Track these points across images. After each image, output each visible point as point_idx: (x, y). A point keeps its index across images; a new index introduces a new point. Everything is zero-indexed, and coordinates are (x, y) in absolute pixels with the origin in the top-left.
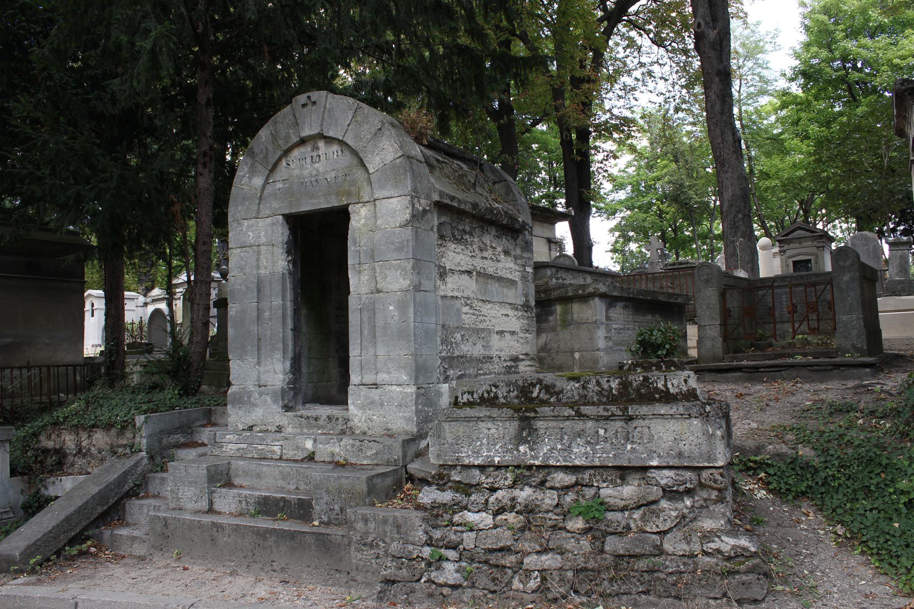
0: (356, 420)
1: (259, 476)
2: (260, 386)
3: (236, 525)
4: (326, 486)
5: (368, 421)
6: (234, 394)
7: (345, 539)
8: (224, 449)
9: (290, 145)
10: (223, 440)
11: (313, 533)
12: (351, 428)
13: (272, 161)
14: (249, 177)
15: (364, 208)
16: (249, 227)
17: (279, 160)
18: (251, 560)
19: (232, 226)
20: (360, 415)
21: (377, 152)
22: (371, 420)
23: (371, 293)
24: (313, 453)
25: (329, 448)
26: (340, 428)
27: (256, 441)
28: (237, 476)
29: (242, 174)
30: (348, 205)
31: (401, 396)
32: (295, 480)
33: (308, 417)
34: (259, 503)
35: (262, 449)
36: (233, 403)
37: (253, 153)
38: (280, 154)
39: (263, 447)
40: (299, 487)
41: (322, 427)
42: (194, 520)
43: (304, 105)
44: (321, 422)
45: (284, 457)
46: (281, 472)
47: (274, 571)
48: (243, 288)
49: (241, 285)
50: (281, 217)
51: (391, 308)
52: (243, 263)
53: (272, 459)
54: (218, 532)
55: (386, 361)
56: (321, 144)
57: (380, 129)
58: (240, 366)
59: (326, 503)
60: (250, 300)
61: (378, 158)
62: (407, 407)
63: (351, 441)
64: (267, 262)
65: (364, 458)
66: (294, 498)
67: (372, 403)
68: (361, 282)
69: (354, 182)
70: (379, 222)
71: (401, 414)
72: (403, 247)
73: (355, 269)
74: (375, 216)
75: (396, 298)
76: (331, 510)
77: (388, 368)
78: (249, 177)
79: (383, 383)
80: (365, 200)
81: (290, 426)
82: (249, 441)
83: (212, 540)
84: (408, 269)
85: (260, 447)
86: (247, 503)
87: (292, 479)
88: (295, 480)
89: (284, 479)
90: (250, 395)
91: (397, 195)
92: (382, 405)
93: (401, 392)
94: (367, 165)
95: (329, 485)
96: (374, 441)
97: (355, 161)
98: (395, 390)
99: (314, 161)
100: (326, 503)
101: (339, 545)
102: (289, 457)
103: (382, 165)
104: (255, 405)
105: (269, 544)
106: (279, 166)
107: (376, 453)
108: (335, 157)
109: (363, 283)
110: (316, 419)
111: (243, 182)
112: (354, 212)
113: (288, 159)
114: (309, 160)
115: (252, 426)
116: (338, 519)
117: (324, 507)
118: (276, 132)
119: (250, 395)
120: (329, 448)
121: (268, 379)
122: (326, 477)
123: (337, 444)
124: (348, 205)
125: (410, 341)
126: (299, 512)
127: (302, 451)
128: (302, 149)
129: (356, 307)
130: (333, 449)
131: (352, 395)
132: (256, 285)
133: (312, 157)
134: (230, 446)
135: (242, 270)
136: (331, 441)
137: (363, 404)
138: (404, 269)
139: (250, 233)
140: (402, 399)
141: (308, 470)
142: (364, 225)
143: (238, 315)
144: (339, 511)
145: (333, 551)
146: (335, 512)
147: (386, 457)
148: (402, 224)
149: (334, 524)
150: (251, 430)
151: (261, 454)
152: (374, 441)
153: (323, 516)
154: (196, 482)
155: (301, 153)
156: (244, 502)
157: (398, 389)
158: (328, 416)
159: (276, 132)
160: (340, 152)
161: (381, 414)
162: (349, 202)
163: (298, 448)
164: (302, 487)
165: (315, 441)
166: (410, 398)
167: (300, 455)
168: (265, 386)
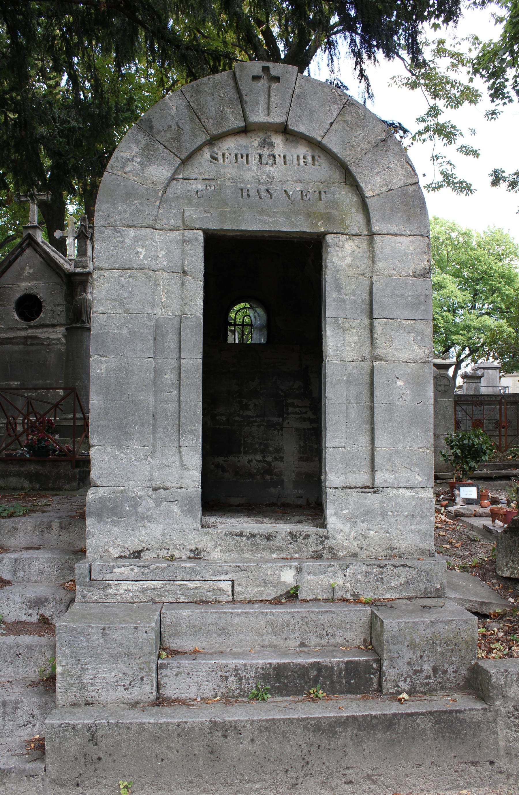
0: (340, 538)
1: (224, 631)
2: (155, 489)
3: (267, 721)
4: (408, 638)
5: (360, 538)
6: (102, 501)
7: (489, 714)
8: (112, 591)
9: (225, 129)
10: (108, 577)
11: (431, 713)
12: (331, 549)
13: (189, 146)
14: (141, 163)
15: (350, 243)
16: (136, 239)
17: (200, 148)
18: (301, 774)
19: (101, 232)
20: (346, 529)
21: (377, 170)
22: (365, 537)
23: (362, 361)
24: (297, 588)
25: (326, 580)
26: (312, 549)
27: (180, 576)
28: (177, 634)
29: (126, 155)
30: (325, 234)
31: (414, 503)
32: (298, 633)
33: (253, 536)
34: (265, 677)
35: (196, 588)
36: (100, 515)
37: (151, 128)
38: (204, 139)
39: (198, 584)
40: (307, 643)
41: (280, 549)
42: (168, 724)
43: (256, 78)
44: (277, 542)
45: (238, 598)
46: (270, 623)
47: (351, 782)
48: (125, 332)
49: (120, 328)
50: (201, 233)
51: (400, 383)
52: (125, 294)
53: (217, 602)
54: (225, 737)
55: (390, 455)
56: (278, 140)
57: (383, 141)
58: (116, 457)
59: (409, 663)
60: (139, 354)
61: (378, 179)
62: (422, 517)
63: (364, 568)
64: (168, 297)
65: (386, 590)
66: (338, 663)
67: (369, 512)
68: (346, 344)
69: (335, 204)
70: (380, 265)
71: (413, 527)
72: (419, 304)
73: (339, 325)
74: (373, 257)
75: (408, 370)
76: (416, 672)
77: (393, 465)
78: (141, 163)
79: (385, 485)
80: (354, 232)
81: (218, 549)
82: (166, 575)
83: (212, 752)
84: (426, 333)
85: (191, 585)
86: (240, 679)
87: (294, 631)
88: (298, 633)
89: (276, 633)
90: (136, 502)
91: (409, 233)
92: (384, 515)
93: (413, 498)
94: (362, 185)
95: (415, 636)
96: (403, 565)
97: (337, 175)
98: (404, 495)
99: (264, 161)
100: (409, 663)
101: (478, 724)
102: (249, 597)
103: (385, 188)
104: (145, 518)
105: (340, 742)
106: (198, 157)
107: (407, 583)
108: (302, 163)
109: (349, 346)
110: (268, 538)
111: (127, 169)
112: (336, 245)
113: (216, 150)
114: (254, 160)
115: (140, 552)
116: (428, 684)
117: (405, 669)
118: (198, 105)
119: (136, 502)
120: (326, 580)
121: (169, 478)
122: (410, 625)
123: (340, 573)
124: (325, 234)
125: (428, 430)
126: (348, 682)
127: (274, 586)
128: (242, 141)
129: (339, 377)
130: (332, 582)
131: (334, 502)
132: (152, 330)
133: (260, 156)
134: (125, 585)
135: (122, 304)
136: (329, 569)
137: (353, 514)
138: (420, 333)
139: (139, 249)
140: (416, 506)
141: (325, 615)
142: (350, 265)
143: (113, 375)
144: (431, 673)
145: (465, 735)
146: (424, 674)
147: (422, 586)
148: (418, 273)
149: (422, 692)
150: (139, 557)
151: (195, 595)
152: (403, 565)
153: (401, 684)
154: (129, 655)
155: (241, 146)
156: (232, 678)
157: (408, 494)
158: (290, 533)
159: (198, 105)
160: (309, 158)
161: (381, 529)
162: (329, 230)
163: (265, 582)
164: (312, 641)
165: (299, 570)
166: (428, 506)
167: (271, 593)
168: (166, 489)
